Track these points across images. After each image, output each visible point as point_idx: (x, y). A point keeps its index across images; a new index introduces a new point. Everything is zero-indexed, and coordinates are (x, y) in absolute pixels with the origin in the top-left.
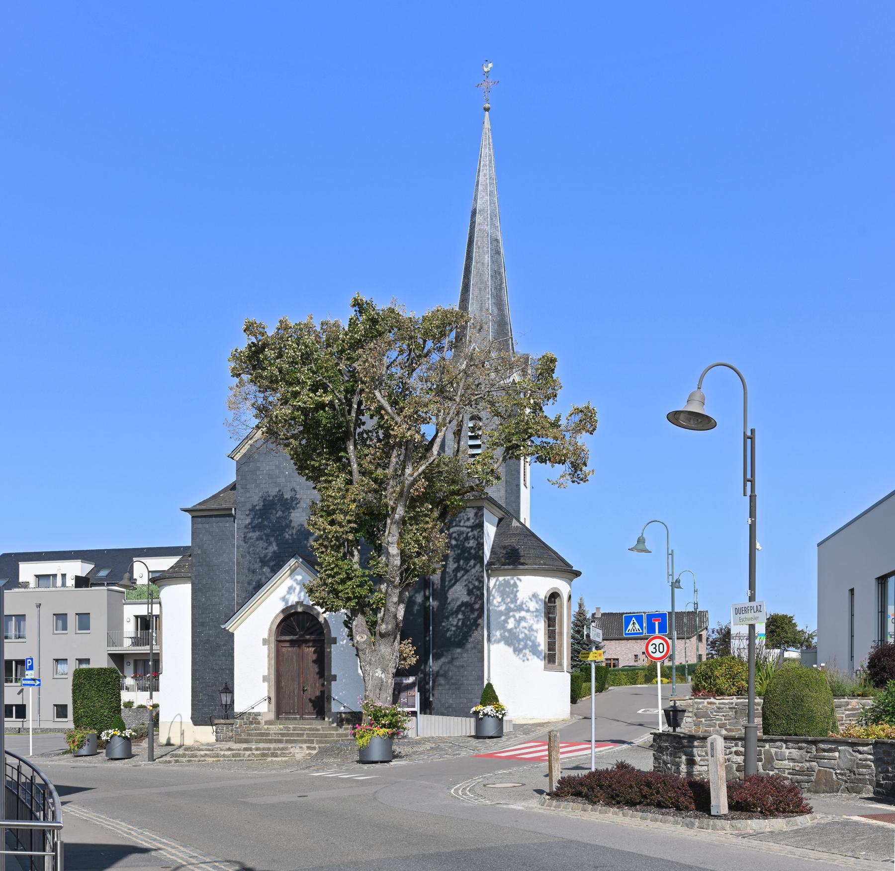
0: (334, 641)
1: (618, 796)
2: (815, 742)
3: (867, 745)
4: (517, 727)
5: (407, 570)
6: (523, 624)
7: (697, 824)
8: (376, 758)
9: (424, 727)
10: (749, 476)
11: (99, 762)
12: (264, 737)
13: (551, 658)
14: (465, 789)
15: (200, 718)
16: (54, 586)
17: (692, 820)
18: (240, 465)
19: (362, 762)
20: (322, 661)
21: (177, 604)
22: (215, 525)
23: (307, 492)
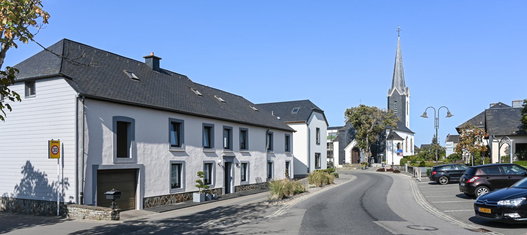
10: (437, 116)
12: (350, 166)
15: (340, 164)
20: (359, 155)
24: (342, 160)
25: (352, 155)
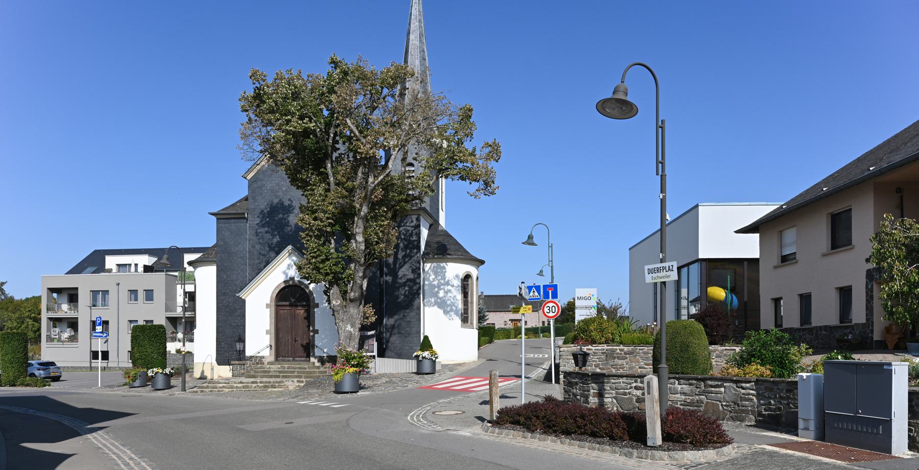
0: (317, 306)
1: (554, 426)
2: (704, 380)
3: (749, 382)
4: (444, 366)
5: (370, 253)
6: (449, 294)
7: (635, 454)
8: (347, 389)
9: (381, 366)
10: (660, 159)
11: (146, 393)
13: (465, 319)
14: (418, 416)
15: (222, 360)
16: (130, 271)
17: (630, 450)
18: (251, 182)
19: (337, 392)
20: (309, 318)
21: (206, 280)
22: (233, 225)
23: (296, 197)
24: (230, 345)
25: (278, 320)
